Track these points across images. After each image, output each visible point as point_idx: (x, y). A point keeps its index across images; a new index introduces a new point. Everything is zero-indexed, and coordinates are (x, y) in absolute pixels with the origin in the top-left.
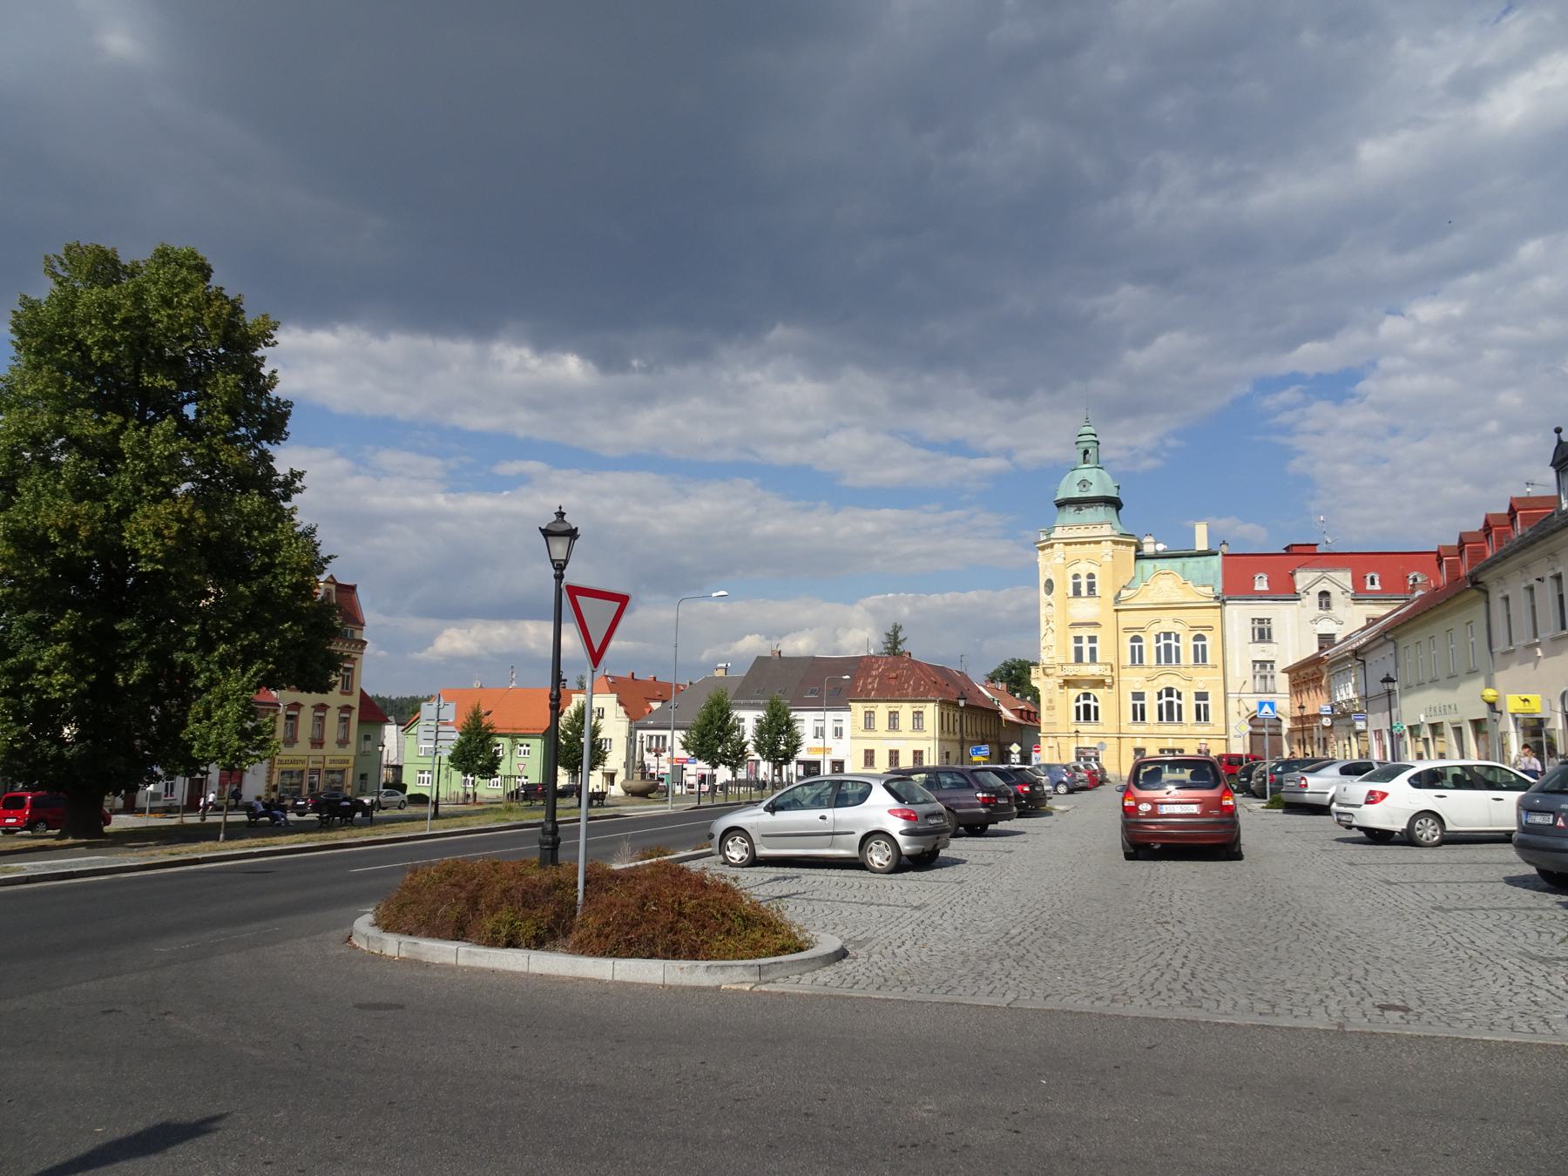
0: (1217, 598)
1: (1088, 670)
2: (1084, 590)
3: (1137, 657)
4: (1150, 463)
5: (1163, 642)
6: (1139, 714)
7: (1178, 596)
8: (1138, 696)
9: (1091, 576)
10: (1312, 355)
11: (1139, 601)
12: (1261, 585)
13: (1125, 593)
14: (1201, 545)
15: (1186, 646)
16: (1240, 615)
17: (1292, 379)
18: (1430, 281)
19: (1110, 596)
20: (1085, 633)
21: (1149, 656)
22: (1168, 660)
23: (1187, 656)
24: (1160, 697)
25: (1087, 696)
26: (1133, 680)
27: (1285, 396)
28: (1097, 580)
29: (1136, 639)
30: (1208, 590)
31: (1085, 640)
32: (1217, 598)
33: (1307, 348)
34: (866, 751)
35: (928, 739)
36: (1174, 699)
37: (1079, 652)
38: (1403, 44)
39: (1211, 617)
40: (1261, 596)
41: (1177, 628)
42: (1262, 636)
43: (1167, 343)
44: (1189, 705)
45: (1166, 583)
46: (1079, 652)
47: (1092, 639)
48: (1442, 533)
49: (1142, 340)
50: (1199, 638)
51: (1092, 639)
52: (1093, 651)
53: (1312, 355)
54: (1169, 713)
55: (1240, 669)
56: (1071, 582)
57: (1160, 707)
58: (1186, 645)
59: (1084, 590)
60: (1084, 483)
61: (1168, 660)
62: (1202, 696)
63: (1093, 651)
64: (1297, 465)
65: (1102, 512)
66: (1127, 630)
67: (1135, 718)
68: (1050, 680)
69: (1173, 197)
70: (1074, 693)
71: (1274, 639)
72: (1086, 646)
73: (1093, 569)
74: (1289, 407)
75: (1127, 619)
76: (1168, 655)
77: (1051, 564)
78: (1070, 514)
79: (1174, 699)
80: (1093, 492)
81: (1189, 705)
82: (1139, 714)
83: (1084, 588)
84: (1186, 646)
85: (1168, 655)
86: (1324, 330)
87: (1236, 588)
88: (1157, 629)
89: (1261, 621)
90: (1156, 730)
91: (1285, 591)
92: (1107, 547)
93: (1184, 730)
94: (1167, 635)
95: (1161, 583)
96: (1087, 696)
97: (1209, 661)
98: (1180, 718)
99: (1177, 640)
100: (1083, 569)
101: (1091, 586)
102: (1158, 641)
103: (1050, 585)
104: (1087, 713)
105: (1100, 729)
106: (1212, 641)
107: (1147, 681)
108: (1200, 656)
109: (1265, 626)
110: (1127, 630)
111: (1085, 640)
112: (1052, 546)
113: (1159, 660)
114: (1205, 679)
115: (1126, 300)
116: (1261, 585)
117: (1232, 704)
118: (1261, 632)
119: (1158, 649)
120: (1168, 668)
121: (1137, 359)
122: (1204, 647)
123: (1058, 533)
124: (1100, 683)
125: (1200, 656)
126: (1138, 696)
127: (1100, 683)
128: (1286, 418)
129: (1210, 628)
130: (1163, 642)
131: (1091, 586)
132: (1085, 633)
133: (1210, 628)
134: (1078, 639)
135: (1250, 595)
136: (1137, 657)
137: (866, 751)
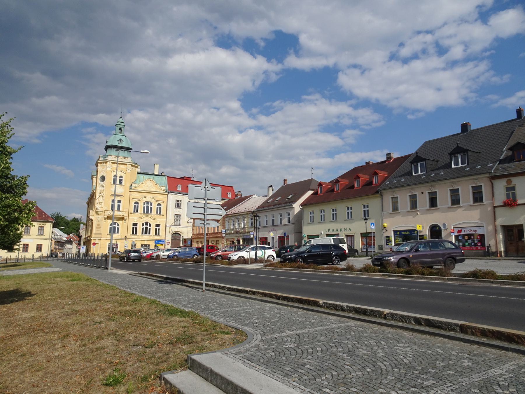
0: (166, 191)
1: (117, 214)
2: (118, 182)
3: (136, 210)
4: (37, 141)
5: (146, 205)
6: (135, 231)
7: (153, 189)
8: (135, 225)
9: (121, 177)
10: (101, 118)
11: (139, 189)
12: (179, 189)
13: (133, 185)
14: (156, 172)
15: (154, 207)
16: (173, 198)
17: (95, 124)
18: (141, 106)
19: (128, 185)
20: (117, 198)
21: (141, 210)
22: (147, 212)
23: (154, 211)
24: (143, 225)
25: (115, 223)
26: (134, 218)
27: (90, 130)
28: (123, 179)
29: (159, 205)
30: (164, 188)
31: (116, 201)
32: (166, 191)
33: (101, 115)
34: (38, 245)
35: (46, 239)
36: (148, 226)
37: (113, 206)
38: (149, 32)
39: (164, 198)
40: (180, 193)
41: (152, 200)
42: (178, 206)
43: (53, 99)
44: (153, 228)
45: (148, 184)
46: (113, 206)
47: (119, 201)
48: (327, 178)
49: (41, 95)
50: (159, 205)
51: (119, 201)
52: (119, 206)
53: (101, 118)
54: (146, 231)
55: (171, 218)
56: (113, 178)
57: (143, 229)
58: (154, 207)
59: (118, 182)
60: (121, 141)
61: (147, 212)
62: (158, 226)
63: (119, 206)
64: (89, 153)
65: (126, 153)
66: (133, 199)
67: (133, 233)
68: (99, 216)
69: (66, 46)
70: (110, 222)
71: (182, 207)
72: (116, 204)
73: (122, 174)
74: (91, 133)
75: (134, 195)
76: (148, 210)
77: (106, 169)
78: (113, 151)
79: (148, 226)
80: (124, 145)
81: (153, 228)
82: (135, 231)
83: (118, 181)
84: (154, 207)
85: (148, 210)
86: (109, 111)
87: (172, 189)
88: (144, 200)
89: (178, 201)
90: (141, 237)
91: (185, 191)
92: (129, 167)
93: (151, 238)
94: (148, 203)
95: (148, 183)
96: (115, 223)
97: (162, 213)
98: (149, 233)
99: (151, 205)
100: (119, 174)
101: (121, 181)
102: (144, 204)
103: (103, 178)
104: (113, 230)
105: (120, 237)
106: (163, 206)
107: (140, 219)
108: (159, 212)
109: (179, 203)
110: (133, 199)
111: (116, 201)
112: (106, 163)
113: (144, 212)
114: (160, 220)
115: (37, 78)
116: (179, 189)
117: (168, 229)
118: (178, 204)
119: (144, 207)
120: (147, 214)
121: (36, 101)
122: (160, 208)
123: (110, 158)
124: (122, 219)
125: (159, 212)
126: (135, 225)
127: (122, 219)
128: (89, 136)
129: (163, 201)
130: (146, 205)
131: (121, 181)
132: (117, 198)
133: (163, 201)
134: (113, 201)
135: (176, 192)
136: (136, 210)
137: (38, 245)
